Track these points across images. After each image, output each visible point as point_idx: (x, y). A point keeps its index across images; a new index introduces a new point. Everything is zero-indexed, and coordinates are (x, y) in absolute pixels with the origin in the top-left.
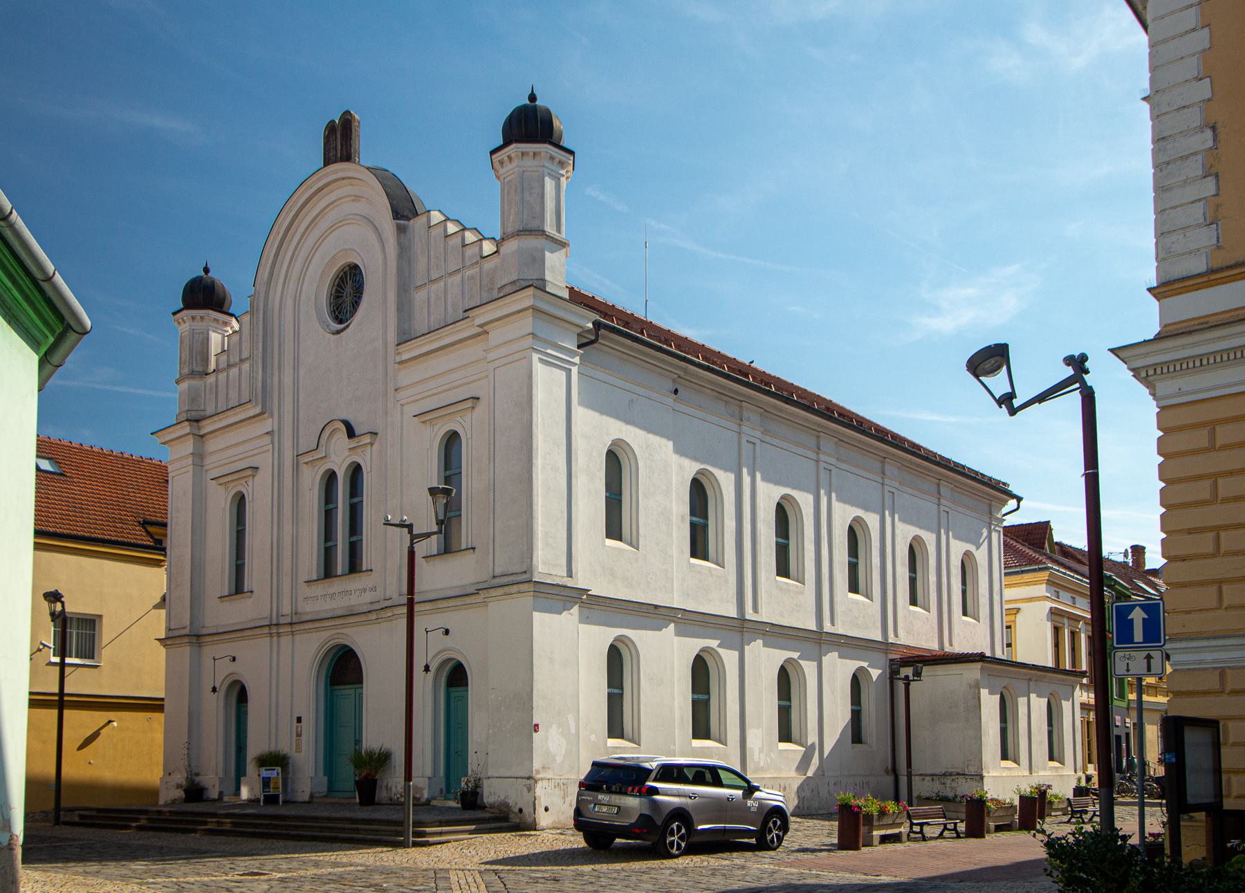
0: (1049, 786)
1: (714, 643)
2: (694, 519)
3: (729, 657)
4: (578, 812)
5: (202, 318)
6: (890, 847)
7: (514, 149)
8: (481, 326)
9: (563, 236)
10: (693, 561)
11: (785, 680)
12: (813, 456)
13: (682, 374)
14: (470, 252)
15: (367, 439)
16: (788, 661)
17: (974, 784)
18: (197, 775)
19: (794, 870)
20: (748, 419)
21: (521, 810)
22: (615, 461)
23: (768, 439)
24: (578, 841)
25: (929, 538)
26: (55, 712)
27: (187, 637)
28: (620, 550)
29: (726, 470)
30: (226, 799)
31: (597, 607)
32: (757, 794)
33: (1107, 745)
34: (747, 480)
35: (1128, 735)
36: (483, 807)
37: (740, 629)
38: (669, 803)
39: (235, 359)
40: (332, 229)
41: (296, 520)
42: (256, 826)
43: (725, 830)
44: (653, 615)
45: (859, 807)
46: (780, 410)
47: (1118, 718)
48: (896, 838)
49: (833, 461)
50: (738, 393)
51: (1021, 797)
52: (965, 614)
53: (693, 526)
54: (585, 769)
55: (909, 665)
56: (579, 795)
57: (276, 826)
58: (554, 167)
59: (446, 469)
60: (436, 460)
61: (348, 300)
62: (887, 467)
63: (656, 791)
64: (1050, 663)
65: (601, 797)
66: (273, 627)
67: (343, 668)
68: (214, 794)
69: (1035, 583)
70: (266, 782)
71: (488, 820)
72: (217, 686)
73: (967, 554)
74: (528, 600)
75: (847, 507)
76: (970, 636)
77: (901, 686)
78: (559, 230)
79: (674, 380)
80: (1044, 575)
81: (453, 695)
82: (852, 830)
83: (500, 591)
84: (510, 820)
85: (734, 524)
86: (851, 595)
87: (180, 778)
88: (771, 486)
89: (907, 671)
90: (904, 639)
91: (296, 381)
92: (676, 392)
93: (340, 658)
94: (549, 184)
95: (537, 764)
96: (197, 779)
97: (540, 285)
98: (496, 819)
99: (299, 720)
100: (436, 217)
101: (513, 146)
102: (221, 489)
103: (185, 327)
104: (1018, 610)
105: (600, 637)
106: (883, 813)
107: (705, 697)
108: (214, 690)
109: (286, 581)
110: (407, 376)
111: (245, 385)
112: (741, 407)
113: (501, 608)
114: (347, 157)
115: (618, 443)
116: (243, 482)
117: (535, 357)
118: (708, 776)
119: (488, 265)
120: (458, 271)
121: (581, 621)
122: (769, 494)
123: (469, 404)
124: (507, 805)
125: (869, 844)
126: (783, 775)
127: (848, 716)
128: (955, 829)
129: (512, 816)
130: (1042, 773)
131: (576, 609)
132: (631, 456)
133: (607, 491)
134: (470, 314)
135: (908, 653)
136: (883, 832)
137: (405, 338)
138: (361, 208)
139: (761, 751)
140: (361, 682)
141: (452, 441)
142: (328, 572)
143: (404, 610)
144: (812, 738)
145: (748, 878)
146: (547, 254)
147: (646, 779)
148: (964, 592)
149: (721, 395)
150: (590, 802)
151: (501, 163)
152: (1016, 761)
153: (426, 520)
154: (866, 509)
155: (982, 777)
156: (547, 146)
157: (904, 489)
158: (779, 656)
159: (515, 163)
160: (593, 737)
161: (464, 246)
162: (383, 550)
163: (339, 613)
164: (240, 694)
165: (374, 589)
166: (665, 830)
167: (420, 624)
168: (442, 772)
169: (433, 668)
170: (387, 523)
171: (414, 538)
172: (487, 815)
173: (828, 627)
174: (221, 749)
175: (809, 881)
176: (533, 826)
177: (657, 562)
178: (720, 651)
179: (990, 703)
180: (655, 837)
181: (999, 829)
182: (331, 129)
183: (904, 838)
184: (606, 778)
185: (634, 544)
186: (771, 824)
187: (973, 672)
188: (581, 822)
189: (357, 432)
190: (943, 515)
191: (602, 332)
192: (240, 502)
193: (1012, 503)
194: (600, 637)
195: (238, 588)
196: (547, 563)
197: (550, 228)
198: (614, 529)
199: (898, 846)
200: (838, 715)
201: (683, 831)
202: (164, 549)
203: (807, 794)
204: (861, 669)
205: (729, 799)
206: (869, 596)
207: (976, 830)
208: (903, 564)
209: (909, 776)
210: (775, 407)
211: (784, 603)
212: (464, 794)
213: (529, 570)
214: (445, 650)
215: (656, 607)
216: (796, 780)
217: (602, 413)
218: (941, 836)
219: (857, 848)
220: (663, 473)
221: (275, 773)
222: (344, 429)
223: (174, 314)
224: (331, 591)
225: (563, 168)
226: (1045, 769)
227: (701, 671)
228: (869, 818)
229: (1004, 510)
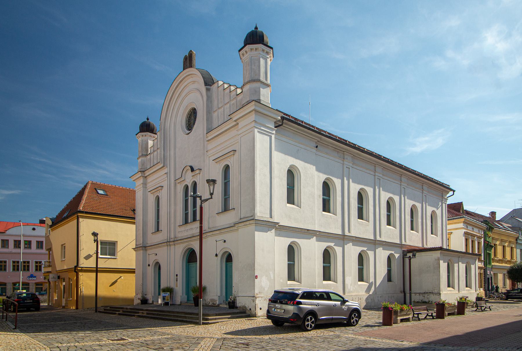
0: (467, 297)
1: (332, 244)
2: (325, 197)
3: (338, 250)
4: (268, 311)
5: (145, 135)
6: (405, 324)
7: (248, 47)
8: (235, 121)
9: (269, 82)
10: (324, 213)
11: (361, 258)
12: (373, 173)
13: (319, 140)
14: (233, 94)
16: (362, 251)
17: (437, 296)
18: (146, 295)
19: (363, 338)
20: (347, 159)
21: (250, 309)
22: (291, 174)
23: (355, 167)
24: (269, 323)
25: (418, 205)
26: (95, 274)
27: (142, 247)
28: (293, 208)
29: (338, 178)
30: (154, 303)
31: (282, 230)
32: (347, 303)
33: (487, 282)
34: (346, 182)
35: (491, 277)
36: (237, 308)
37: (343, 239)
38: (307, 308)
39: (155, 149)
40: (186, 96)
41: (175, 204)
42: (153, 314)
43: (332, 319)
44: (307, 233)
45: (392, 308)
46: (360, 155)
47: (488, 271)
48: (407, 320)
49: (381, 176)
50: (343, 148)
51: (458, 302)
52: (432, 234)
53: (324, 200)
54: (271, 294)
56: (269, 304)
57: (160, 315)
58: (265, 54)
59: (225, 180)
60: (221, 176)
61: (192, 122)
62: (402, 178)
63: (300, 303)
64: (464, 251)
65: (277, 305)
66: (169, 242)
67: (191, 257)
68: (151, 302)
69: (458, 223)
70: (164, 298)
71: (237, 313)
73: (433, 212)
74: (253, 227)
75: (387, 193)
76: (434, 241)
77: (407, 260)
78: (266, 80)
79: (316, 143)
80: (463, 220)
81: (228, 265)
82: (389, 318)
83: (243, 224)
84: (246, 313)
85: (341, 199)
86: (388, 226)
87: (140, 296)
88: (356, 185)
89: (410, 255)
90: (408, 243)
91: (175, 154)
92: (317, 147)
93: (191, 253)
94: (262, 61)
95: (257, 291)
96: (146, 296)
97: (258, 101)
98: (241, 313)
99: (177, 275)
100: (221, 83)
101: (247, 46)
102: (152, 195)
103: (140, 140)
104: (452, 233)
105: (285, 242)
106: (402, 310)
107: (329, 265)
108: (216, 255)
109: (172, 226)
110: (211, 146)
111: (159, 158)
112: (344, 154)
113: (243, 231)
114: (191, 66)
115: (292, 166)
117: (256, 130)
118: (325, 296)
119: (239, 98)
120: (228, 102)
121: (276, 235)
122: (355, 188)
124: (245, 307)
125: (396, 323)
126: (360, 294)
127: (386, 272)
128: (432, 315)
129: (247, 311)
130: (463, 292)
131: (273, 230)
132: (298, 172)
133: (288, 185)
134: (231, 116)
135: (410, 248)
136: (402, 318)
137: (209, 131)
138: (196, 86)
139: (351, 285)
142: (186, 222)
143: (203, 232)
144: (372, 280)
145: (340, 344)
146: (261, 89)
147: (296, 298)
148: (432, 226)
149: (335, 149)
150: (273, 307)
151: (243, 55)
152: (453, 288)
154: (394, 194)
155: (440, 294)
156: (261, 45)
157: (409, 187)
158: (359, 249)
159: (248, 53)
160: (281, 281)
161: (230, 92)
163: (189, 236)
164: (158, 266)
166: (305, 319)
168: (224, 294)
172: (238, 311)
173: (378, 238)
174: (153, 286)
175: (369, 346)
176: (255, 316)
177: (308, 212)
178: (335, 247)
179: (443, 266)
180: (297, 323)
181: (449, 314)
182: (186, 58)
183: (411, 319)
184: (281, 297)
185: (299, 206)
186: (353, 316)
187: (438, 254)
188: (269, 316)
190: (424, 197)
191: (285, 121)
192: (158, 199)
193: (451, 193)
194: (285, 242)
195: (158, 230)
196: (261, 212)
197: (262, 78)
198: (291, 199)
199: (408, 323)
200: (382, 271)
201: (313, 319)
203: (370, 301)
204: (391, 254)
205: (335, 306)
206: (395, 227)
207: (440, 315)
208: (408, 215)
209: (410, 293)
210: (358, 154)
211: (361, 229)
212: (229, 303)
213: (254, 215)
214: (224, 248)
215: (308, 230)
216: (365, 296)
217: (286, 154)
218: (425, 318)
219: (391, 325)
220: (311, 179)
221: (167, 294)
224: (187, 229)
225: (268, 55)
226: (464, 290)
227: (327, 255)
228: (396, 312)
229: (448, 195)
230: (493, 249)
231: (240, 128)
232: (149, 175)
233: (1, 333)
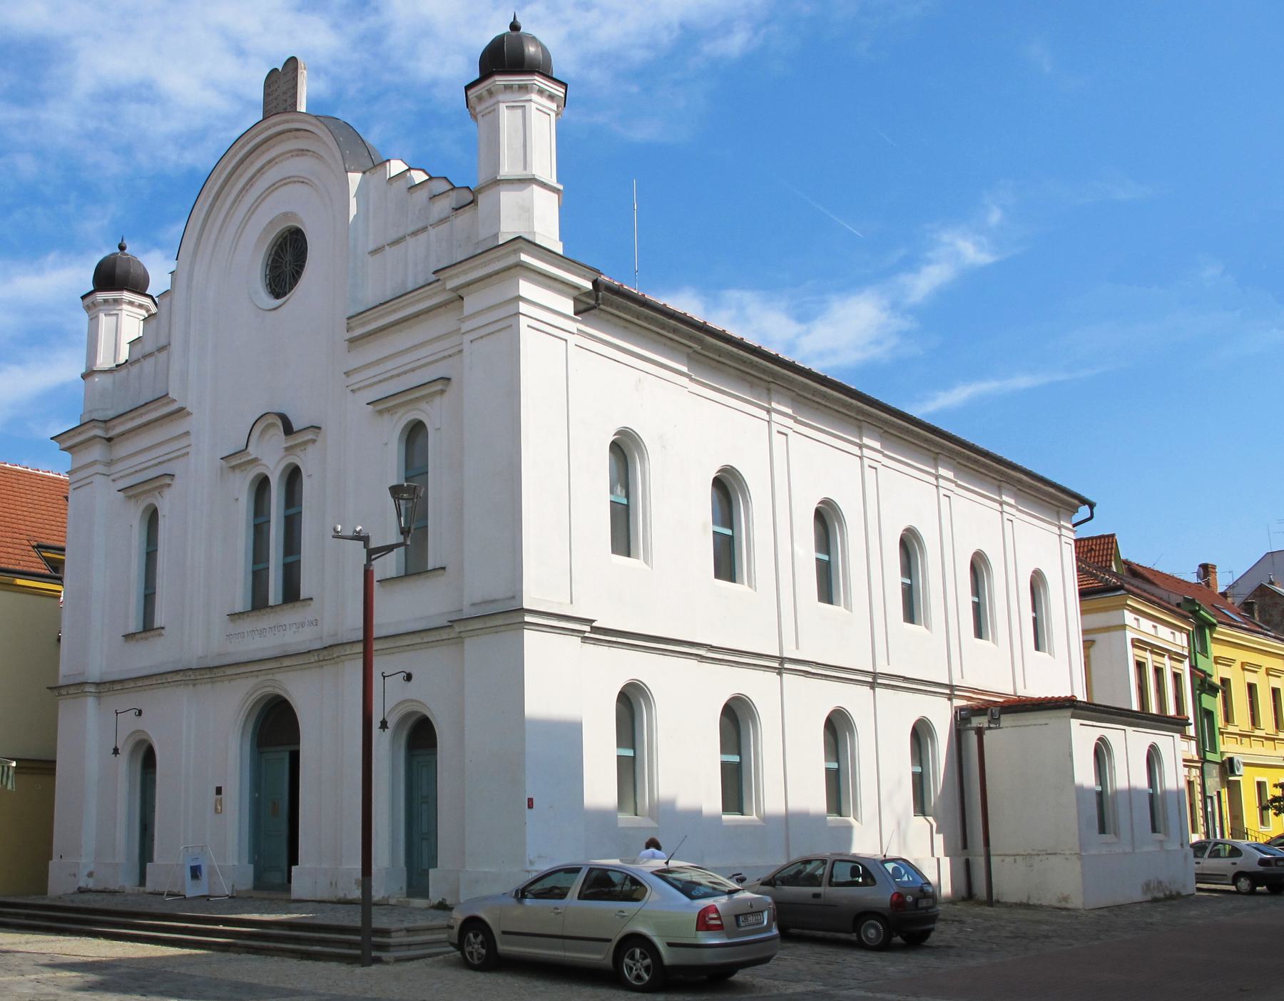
8: (453, 290)
15: (309, 436)
40: (273, 188)
55: (980, 715)
61: (288, 269)
89: (977, 721)
99: (219, 791)
108: (116, 751)
123: (438, 387)
134: (442, 275)
141: (415, 433)
143: (360, 648)
153: (386, 530)
162: (331, 575)
165: (315, 623)
167: (380, 665)
169: (391, 724)
170: (337, 536)
171: (372, 553)
177: (670, 580)
189: (296, 427)
193: (1084, 511)
195: (148, 626)
202: (60, 579)
214: (405, 701)
222: (279, 423)
223: (83, 298)
230: (1220, 695)
232: (123, 434)
233: (1279, 852)
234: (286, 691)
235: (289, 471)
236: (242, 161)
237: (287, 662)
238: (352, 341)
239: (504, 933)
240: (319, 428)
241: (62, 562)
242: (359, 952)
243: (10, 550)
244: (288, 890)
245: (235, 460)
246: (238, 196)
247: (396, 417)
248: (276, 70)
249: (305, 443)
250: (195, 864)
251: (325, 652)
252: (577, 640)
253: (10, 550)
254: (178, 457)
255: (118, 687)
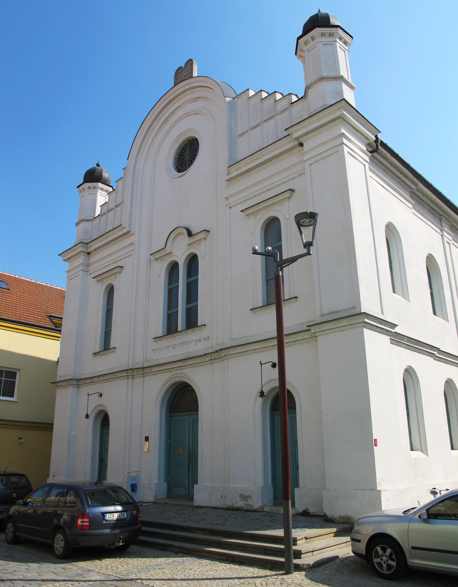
8: (297, 139)
15: (203, 235)
40: (180, 119)
66: (130, 373)
72: (89, 414)
108: (87, 416)
116: (113, 277)
123: (287, 194)
134: (290, 131)
140: (197, 410)
151: (306, 43)
164: (104, 420)
192: (110, 291)
195: (106, 346)
202: (60, 331)
214: (100, 405)
223: (78, 187)
231: (305, 150)
232: (96, 250)
234: (189, 379)
235: (189, 259)
236: (163, 109)
237: (190, 362)
238: (229, 180)
239: (413, 548)
240: (209, 231)
241: (62, 324)
242: (283, 560)
243: (35, 316)
244: (191, 498)
245: (156, 255)
246: (160, 127)
247: (258, 217)
248: (181, 67)
249: (200, 240)
250: (133, 482)
251: (216, 354)
252: (387, 339)
253: (35, 316)
254: (125, 258)
255: (90, 381)
